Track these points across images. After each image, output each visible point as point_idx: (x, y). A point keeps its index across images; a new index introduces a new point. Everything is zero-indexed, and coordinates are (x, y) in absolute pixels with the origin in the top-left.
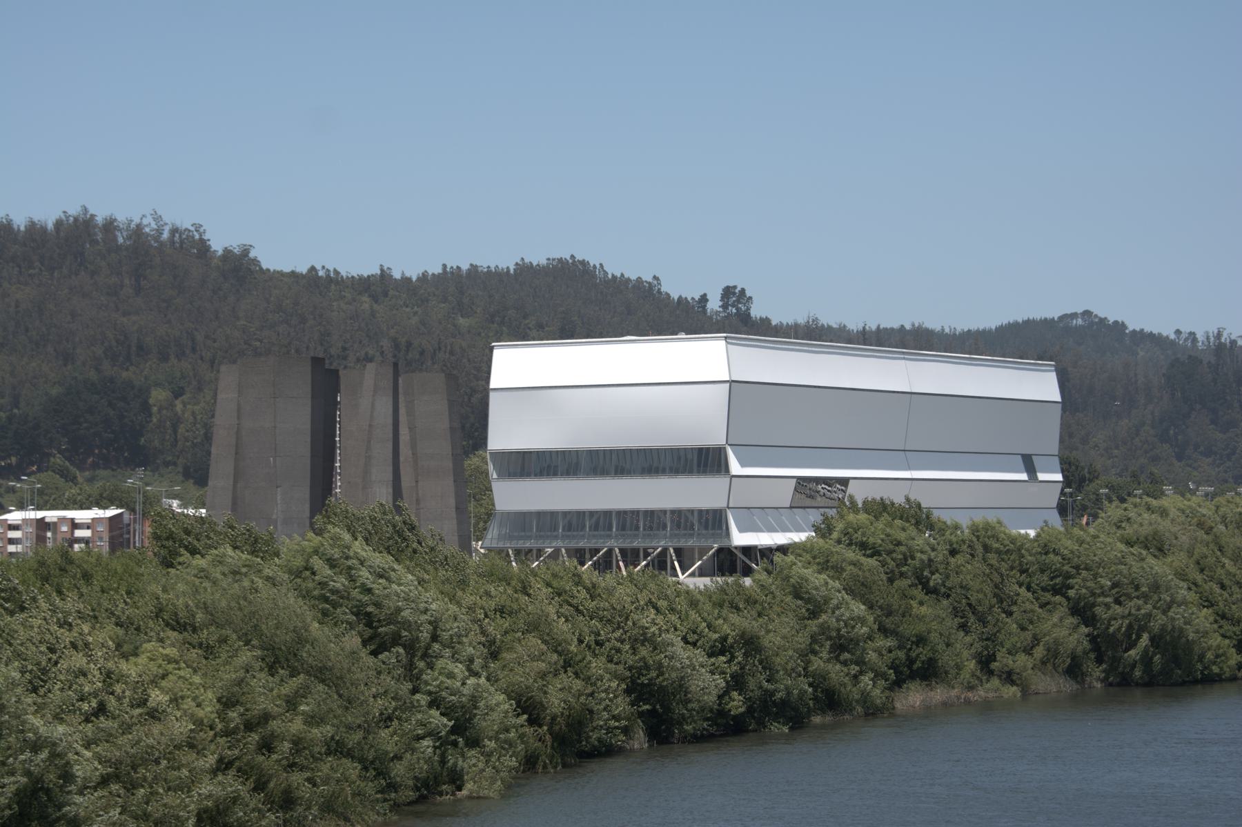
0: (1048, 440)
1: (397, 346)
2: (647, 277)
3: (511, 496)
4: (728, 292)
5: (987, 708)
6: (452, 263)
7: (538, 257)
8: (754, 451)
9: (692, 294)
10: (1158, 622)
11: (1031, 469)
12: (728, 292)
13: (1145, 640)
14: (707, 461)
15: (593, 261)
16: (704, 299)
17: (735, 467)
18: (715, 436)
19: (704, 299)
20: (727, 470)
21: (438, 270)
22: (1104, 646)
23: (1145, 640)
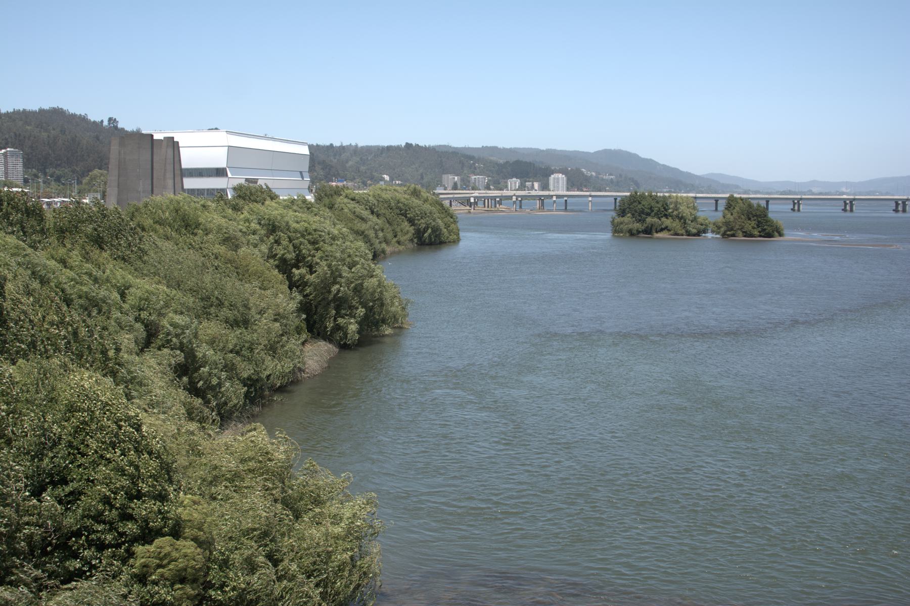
0: (305, 167)
1: (16, 135)
2: (83, 114)
3: (190, 183)
4: (110, 119)
5: (399, 252)
6: (17, 108)
7: (46, 107)
8: (236, 169)
9: (98, 120)
10: (433, 224)
11: (303, 177)
12: (110, 119)
13: (430, 231)
14: (220, 172)
15: (65, 108)
16: (102, 121)
17: (229, 175)
18: (222, 164)
19: (102, 121)
20: (227, 175)
21: (12, 110)
22: (419, 234)
23: (430, 231)
